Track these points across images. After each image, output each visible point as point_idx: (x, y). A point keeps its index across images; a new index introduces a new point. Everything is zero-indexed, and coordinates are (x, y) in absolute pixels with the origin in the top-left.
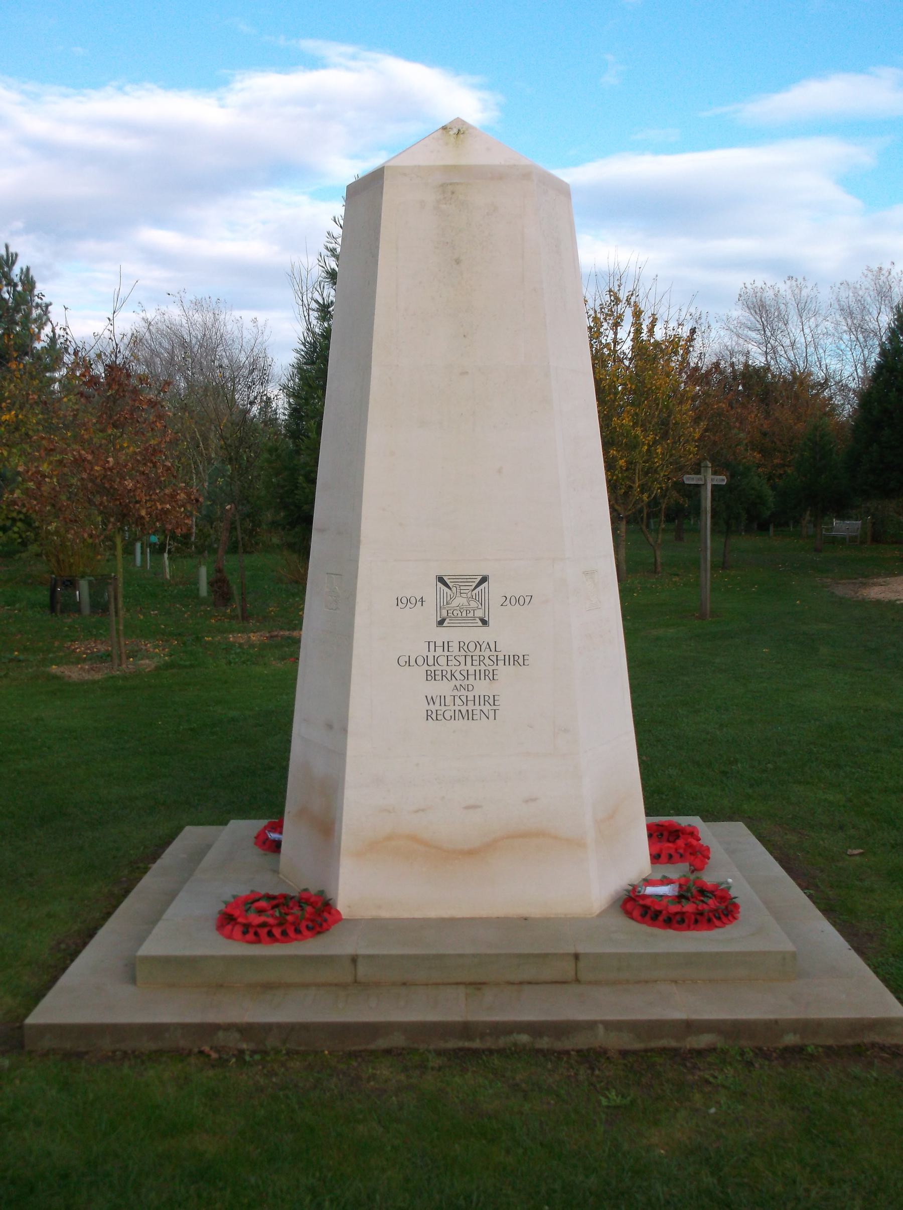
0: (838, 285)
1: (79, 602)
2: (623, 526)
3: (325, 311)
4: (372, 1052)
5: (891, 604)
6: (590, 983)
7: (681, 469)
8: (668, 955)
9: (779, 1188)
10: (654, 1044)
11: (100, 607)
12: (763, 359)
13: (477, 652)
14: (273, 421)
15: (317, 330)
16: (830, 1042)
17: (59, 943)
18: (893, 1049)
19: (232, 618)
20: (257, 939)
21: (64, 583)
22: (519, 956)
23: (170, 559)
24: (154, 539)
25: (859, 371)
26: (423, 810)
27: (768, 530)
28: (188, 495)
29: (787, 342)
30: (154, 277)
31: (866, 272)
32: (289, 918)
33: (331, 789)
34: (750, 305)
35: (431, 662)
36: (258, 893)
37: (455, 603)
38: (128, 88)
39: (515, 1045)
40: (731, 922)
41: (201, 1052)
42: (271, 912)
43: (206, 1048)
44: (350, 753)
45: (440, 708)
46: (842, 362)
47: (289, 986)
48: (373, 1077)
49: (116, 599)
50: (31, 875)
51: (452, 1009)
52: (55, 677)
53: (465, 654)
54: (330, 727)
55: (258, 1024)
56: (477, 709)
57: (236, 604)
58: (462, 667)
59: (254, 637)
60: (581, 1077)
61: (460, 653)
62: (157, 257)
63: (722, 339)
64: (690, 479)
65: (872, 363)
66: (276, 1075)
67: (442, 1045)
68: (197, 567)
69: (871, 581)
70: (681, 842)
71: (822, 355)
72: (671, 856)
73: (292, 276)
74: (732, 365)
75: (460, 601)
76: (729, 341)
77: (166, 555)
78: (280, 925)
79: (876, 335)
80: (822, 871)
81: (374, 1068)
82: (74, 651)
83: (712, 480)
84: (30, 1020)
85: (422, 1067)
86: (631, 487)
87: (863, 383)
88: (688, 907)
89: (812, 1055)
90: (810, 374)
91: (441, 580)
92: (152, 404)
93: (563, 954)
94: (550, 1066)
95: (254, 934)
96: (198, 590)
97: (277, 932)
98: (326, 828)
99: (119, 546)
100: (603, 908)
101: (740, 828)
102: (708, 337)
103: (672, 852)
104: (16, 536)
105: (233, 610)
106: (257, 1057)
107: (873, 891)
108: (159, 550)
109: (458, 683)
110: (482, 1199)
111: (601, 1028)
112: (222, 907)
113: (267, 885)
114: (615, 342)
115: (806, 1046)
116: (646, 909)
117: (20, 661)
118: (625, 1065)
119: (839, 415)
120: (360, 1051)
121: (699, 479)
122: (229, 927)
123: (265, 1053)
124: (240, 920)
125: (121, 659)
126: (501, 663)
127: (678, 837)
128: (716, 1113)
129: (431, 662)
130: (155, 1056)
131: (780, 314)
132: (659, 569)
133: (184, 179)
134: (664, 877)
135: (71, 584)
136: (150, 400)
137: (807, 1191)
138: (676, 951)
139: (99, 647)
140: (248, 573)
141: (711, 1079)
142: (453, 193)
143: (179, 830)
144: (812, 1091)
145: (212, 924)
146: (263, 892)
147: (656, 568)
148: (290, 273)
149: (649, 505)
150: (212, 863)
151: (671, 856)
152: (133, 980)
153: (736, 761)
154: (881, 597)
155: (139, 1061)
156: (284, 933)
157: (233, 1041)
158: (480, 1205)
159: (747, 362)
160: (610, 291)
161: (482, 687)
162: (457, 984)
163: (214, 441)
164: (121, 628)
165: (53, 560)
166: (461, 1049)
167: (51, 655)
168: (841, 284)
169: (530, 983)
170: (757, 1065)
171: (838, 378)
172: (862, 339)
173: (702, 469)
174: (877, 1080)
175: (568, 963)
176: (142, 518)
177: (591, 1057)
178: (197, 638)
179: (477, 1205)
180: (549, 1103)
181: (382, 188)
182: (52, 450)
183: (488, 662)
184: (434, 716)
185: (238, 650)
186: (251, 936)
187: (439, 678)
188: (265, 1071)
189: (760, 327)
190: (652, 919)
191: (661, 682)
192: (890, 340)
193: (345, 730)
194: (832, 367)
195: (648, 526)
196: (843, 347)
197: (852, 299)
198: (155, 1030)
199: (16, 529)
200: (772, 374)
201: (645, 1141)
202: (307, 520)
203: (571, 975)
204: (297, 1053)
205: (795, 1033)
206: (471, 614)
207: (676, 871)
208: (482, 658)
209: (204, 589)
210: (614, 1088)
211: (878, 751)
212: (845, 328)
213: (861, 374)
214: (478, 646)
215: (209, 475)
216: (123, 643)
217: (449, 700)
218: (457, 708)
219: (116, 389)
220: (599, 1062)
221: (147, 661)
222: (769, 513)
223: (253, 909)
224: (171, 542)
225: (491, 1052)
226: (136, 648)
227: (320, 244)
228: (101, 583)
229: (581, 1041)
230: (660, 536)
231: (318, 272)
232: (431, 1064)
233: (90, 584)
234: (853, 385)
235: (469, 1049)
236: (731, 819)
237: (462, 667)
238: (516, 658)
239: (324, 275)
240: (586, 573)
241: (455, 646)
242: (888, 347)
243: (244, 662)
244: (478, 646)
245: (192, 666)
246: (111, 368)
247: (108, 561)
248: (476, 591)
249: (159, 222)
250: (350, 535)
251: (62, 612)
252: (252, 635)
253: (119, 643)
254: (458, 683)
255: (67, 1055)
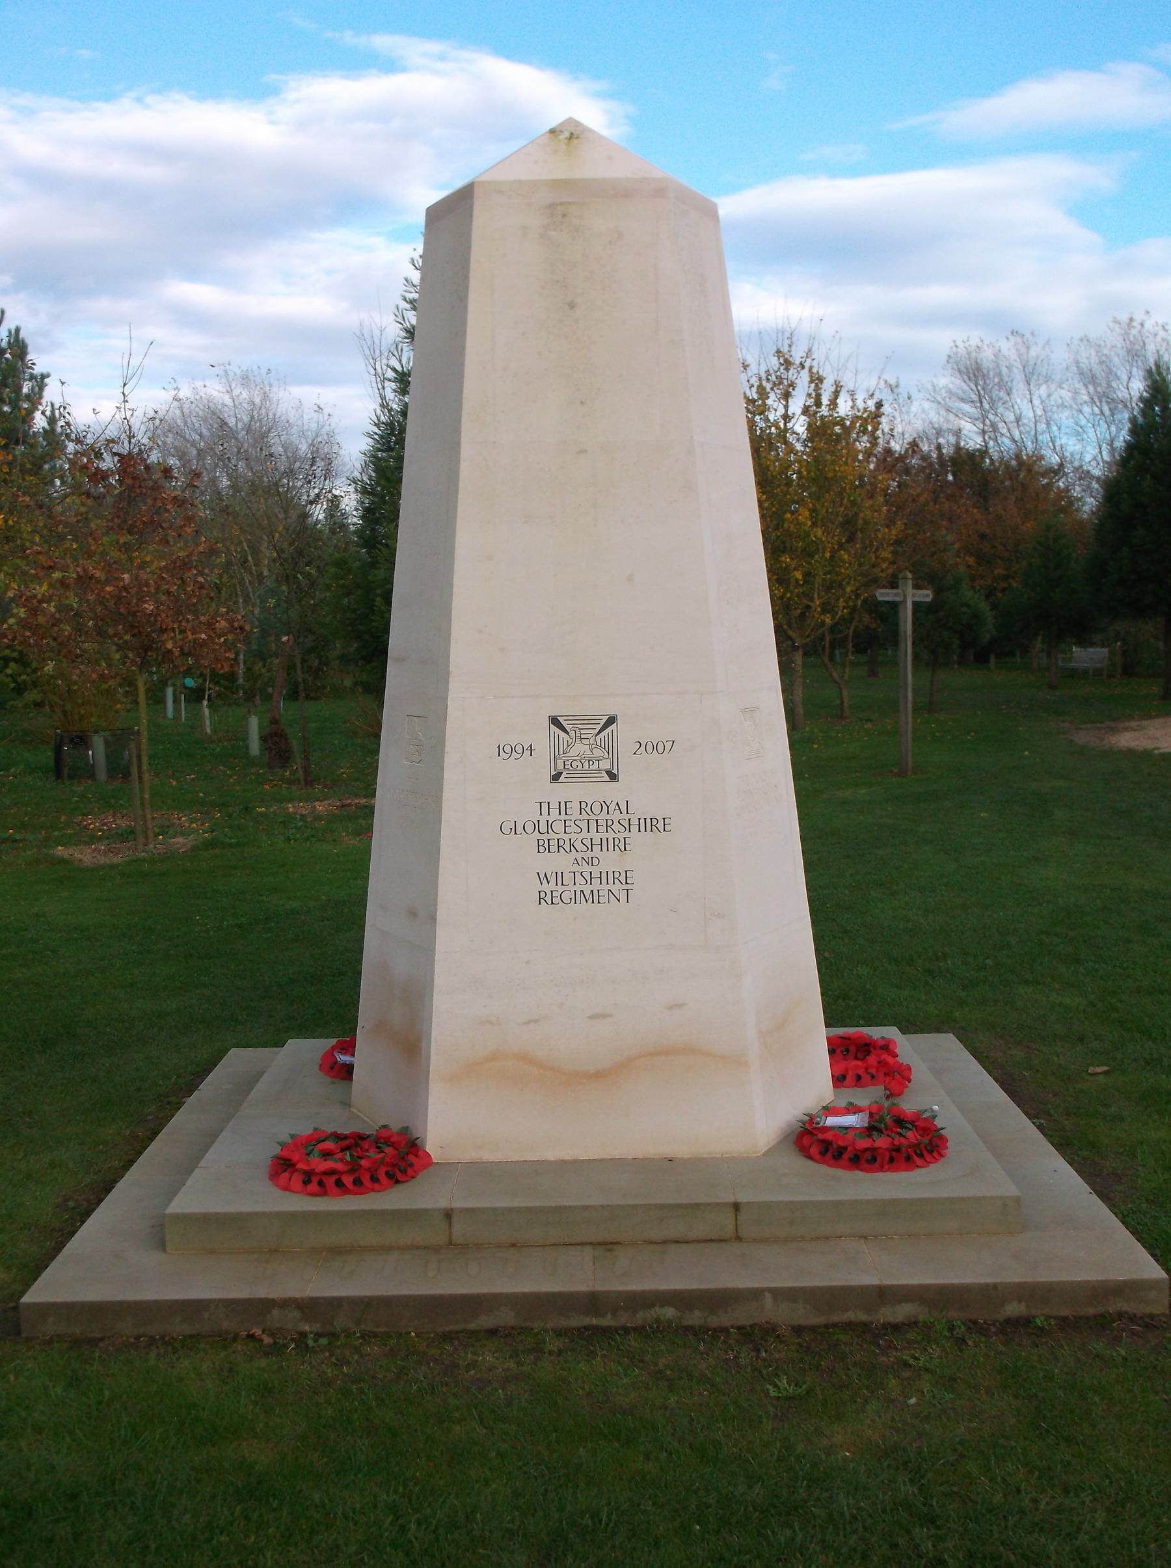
0: (1076, 342)
1: (93, 765)
2: (798, 657)
3: (403, 380)
4: (473, 1334)
5: (1146, 755)
6: (754, 1240)
7: (874, 582)
8: (855, 1203)
9: (998, 1498)
10: (835, 1318)
11: (119, 771)
12: (979, 440)
13: (604, 815)
14: (343, 527)
15: (395, 406)
16: (1065, 1312)
17: (66, 1200)
18: (1147, 1320)
19: (291, 782)
20: (323, 1191)
21: (72, 740)
22: (662, 1207)
23: (209, 707)
24: (189, 682)
25: (1104, 453)
26: (536, 1021)
27: (987, 661)
28: (231, 621)
29: (1010, 417)
30: (185, 343)
31: (1112, 325)
32: (362, 1162)
33: (416, 996)
34: (963, 369)
35: (543, 829)
36: (324, 1131)
37: (573, 752)
38: (149, 99)
39: (658, 1320)
40: (936, 1160)
41: (251, 1336)
42: (339, 1155)
43: (257, 1331)
44: (439, 947)
45: (556, 888)
46: (1082, 442)
47: (363, 1249)
48: (474, 1364)
49: (139, 757)
50: (30, 1114)
51: (576, 1276)
52: (62, 861)
53: (588, 817)
54: (414, 914)
55: (324, 1298)
56: (601, 888)
57: (297, 764)
58: (584, 834)
59: (321, 807)
60: (742, 1361)
61: (581, 817)
62: (189, 318)
63: (921, 413)
64: (884, 595)
65: (1119, 443)
66: (348, 1363)
67: (563, 1323)
68: (246, 718)
69: (1122, 725)
70: (872, 1059)
71: (1056, 433)
72: (859, 1078)
73: (361, 337)
74: (939, 447)
75: (580, 748)
76: (936, 416)
77: (205, 703)
78: (351, 1172)
79: (1125, 406)
80: (1055, 1095)
81: (474, 1354)
82: (86, 827)
83: (913, 595)
84: (26, 1299)
85: (538, 1350)
86: (808, 607)
87: (1110, 471)
88: (881, 1142)
89: (1042, 1329)
90: (1041, 458)
91: (555, 721)
92: (180, 502)
93: (717, 1204)
94: (702, 1348)
95: (319, 1183)
96: (247, 747)
97: (348, 1180)
98: (411, 1046)
99: (142, 690)
100: (772, 1144)
101: (949, 1041)
102: (908, 412)
103: (861, 1072)
104: (9, 679)
105: (294, 772)
106: (324, 1341)
107: (1122, 1119)
108: (196, 696)
109: (579, 856)
110: (614, 1517)
111: (768, 1299)
112: (277, 1150)
113: (336, 1121)
114: (786, 418)
115: (1034, 1317)
116: (826, 1146)
117: (16, 841)
118: (800, 1344)
119: (1078, 510)
120: (457, 1333)
121: (896, 595)
122: (286, 1175)
123: (333, 1336)
124: (300, 1166)
125: (147, 838)
126: (635, 828)
127: (868, 1053)
128: (917, 1404)
129: (543, 829)
130: (191, 1342)
131: (1001, 380)
132: (847, 712)
133: (218, 216)
134: (851, 1104)
135: (82, 741)
136: (175, 498)
137: (1035, 1501)
138: (866, 1198)
139: (118, 822)
140: (312, 725)
141: (911, 1361)
142: (564, 216)
143: (222, 1053)
144: (1041, 1375)
145: (264, 1172)
146: (330, 1129)
147: (842, 710)
148: (358, 333)
149: (832, 629)
150: (265, 1094)
151: (859, 1078)
152: (162, 1245)
153: (945, 956)
154: (1132, 745)
155: (170, 1348)
156: (358, 1182)
157: (292, 1321)
158: (611, 1525)
159: (958, 443)
160: (778, 352)
161: (610, 861)
162: (582, 1244)
163: (268, 553)
164: (147, 796)
165: (59, 711)
166: (586, 1328)
167: (56, 833)
168: (1082, 340)
169: (677, 1242)
170: (970, 1343)
171: (1076, 464)
172: (1107, 412)
173: (901, 582)
174: (1125, 1359)
175: (728, 1216)
176: (170, 651)
177: (756, 1336)
178: (246, 808)
179: (607, 1525)
180: (701, 1394)
181: (471, 208)
182: (51, 567)
183: (618, 827)
184: (548, 899)
185: (300, 824)
186: (313, 1186)
187: (554, 849)
188: (333, 1359)
189: (974, 397)
190: (834, 1157)
191: (848, 857)
192: (1143, 413)
193: (433, 919)
194: (1070, 449)
195: (832, 659)
196: (1083, 422)
197: (1094, 360)
198: (193, 1308)
199: (9, 671)
200: (991, 459)
201: (825, 1441)
202: (384, 652)
203: (729, 1230)
204: (375, 1335)
205: (1019, 1302)
206: (595, 766)
207: (868, 1096)
208: (610, 823)
209: (255, 747)
210: (786, 1374)
211: (1129, 941)
212: (1086, 398)
213: (1106, 457)
214: (605, 807)
215: (259, 596)
216: (149, 816)
217: (568, 878)
218: (578, 888)
219: (134, 488)
220: (766, 1341)
221: (181, 840)
222: (988, 636)
223: (316, 1153)
224: (212, 686)
225: (627, 1330)
226: (167, 823)
227: (395, 295)
228: (119, 739)
229: (742, 1315)
230: (847, 670)
231: (394, 332)
232: (548, 1347)
233: (107, 744)
234: (1097, 472)
235: (597, 1328)
236: (938, 1030)
237: (584, 834)
238: (654, 822)
239: (403, 334)
240: (744, 711)
241: (574, 808)
242: (1140, 420)
243: (307, 839)
244: (605, 807)
245: (238, 844)
246: (127, 462)
247: (128, 711)
248: (601, 735)
249: (193, 273)
250: (436, 666)
251: (71, 777)
252: (317, 804)
253: (144, 816)
254: (579, 856)
255: (76, 1343)
